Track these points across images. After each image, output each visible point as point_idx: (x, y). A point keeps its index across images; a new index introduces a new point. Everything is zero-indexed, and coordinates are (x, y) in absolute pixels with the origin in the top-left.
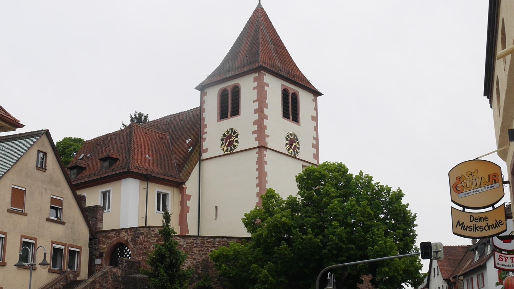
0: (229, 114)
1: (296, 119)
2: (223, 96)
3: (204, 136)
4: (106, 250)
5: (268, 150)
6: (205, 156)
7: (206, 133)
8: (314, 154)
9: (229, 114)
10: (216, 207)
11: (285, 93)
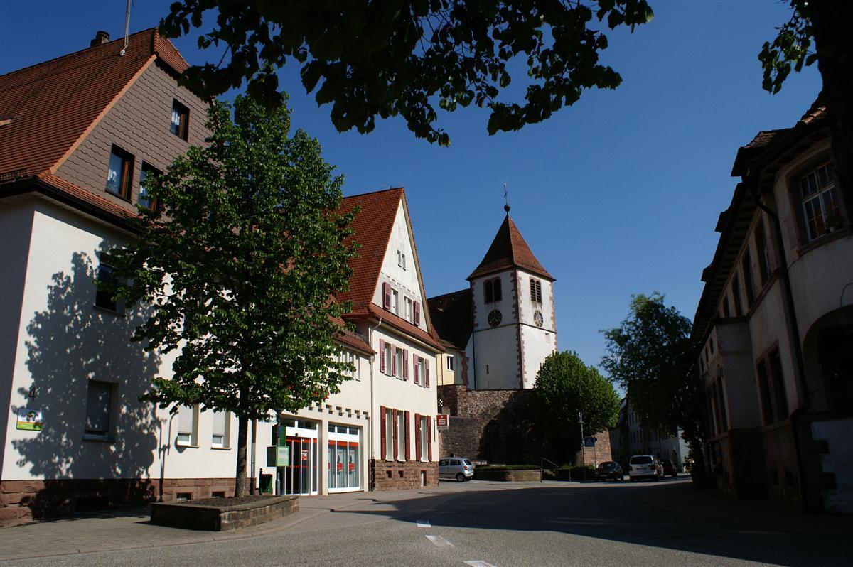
0: (493, 299)
1: (540, 300)
2: (488, 285)
3: (475, 314)
6: (476, 329)
9: (493, 299)
11: (532, 281)
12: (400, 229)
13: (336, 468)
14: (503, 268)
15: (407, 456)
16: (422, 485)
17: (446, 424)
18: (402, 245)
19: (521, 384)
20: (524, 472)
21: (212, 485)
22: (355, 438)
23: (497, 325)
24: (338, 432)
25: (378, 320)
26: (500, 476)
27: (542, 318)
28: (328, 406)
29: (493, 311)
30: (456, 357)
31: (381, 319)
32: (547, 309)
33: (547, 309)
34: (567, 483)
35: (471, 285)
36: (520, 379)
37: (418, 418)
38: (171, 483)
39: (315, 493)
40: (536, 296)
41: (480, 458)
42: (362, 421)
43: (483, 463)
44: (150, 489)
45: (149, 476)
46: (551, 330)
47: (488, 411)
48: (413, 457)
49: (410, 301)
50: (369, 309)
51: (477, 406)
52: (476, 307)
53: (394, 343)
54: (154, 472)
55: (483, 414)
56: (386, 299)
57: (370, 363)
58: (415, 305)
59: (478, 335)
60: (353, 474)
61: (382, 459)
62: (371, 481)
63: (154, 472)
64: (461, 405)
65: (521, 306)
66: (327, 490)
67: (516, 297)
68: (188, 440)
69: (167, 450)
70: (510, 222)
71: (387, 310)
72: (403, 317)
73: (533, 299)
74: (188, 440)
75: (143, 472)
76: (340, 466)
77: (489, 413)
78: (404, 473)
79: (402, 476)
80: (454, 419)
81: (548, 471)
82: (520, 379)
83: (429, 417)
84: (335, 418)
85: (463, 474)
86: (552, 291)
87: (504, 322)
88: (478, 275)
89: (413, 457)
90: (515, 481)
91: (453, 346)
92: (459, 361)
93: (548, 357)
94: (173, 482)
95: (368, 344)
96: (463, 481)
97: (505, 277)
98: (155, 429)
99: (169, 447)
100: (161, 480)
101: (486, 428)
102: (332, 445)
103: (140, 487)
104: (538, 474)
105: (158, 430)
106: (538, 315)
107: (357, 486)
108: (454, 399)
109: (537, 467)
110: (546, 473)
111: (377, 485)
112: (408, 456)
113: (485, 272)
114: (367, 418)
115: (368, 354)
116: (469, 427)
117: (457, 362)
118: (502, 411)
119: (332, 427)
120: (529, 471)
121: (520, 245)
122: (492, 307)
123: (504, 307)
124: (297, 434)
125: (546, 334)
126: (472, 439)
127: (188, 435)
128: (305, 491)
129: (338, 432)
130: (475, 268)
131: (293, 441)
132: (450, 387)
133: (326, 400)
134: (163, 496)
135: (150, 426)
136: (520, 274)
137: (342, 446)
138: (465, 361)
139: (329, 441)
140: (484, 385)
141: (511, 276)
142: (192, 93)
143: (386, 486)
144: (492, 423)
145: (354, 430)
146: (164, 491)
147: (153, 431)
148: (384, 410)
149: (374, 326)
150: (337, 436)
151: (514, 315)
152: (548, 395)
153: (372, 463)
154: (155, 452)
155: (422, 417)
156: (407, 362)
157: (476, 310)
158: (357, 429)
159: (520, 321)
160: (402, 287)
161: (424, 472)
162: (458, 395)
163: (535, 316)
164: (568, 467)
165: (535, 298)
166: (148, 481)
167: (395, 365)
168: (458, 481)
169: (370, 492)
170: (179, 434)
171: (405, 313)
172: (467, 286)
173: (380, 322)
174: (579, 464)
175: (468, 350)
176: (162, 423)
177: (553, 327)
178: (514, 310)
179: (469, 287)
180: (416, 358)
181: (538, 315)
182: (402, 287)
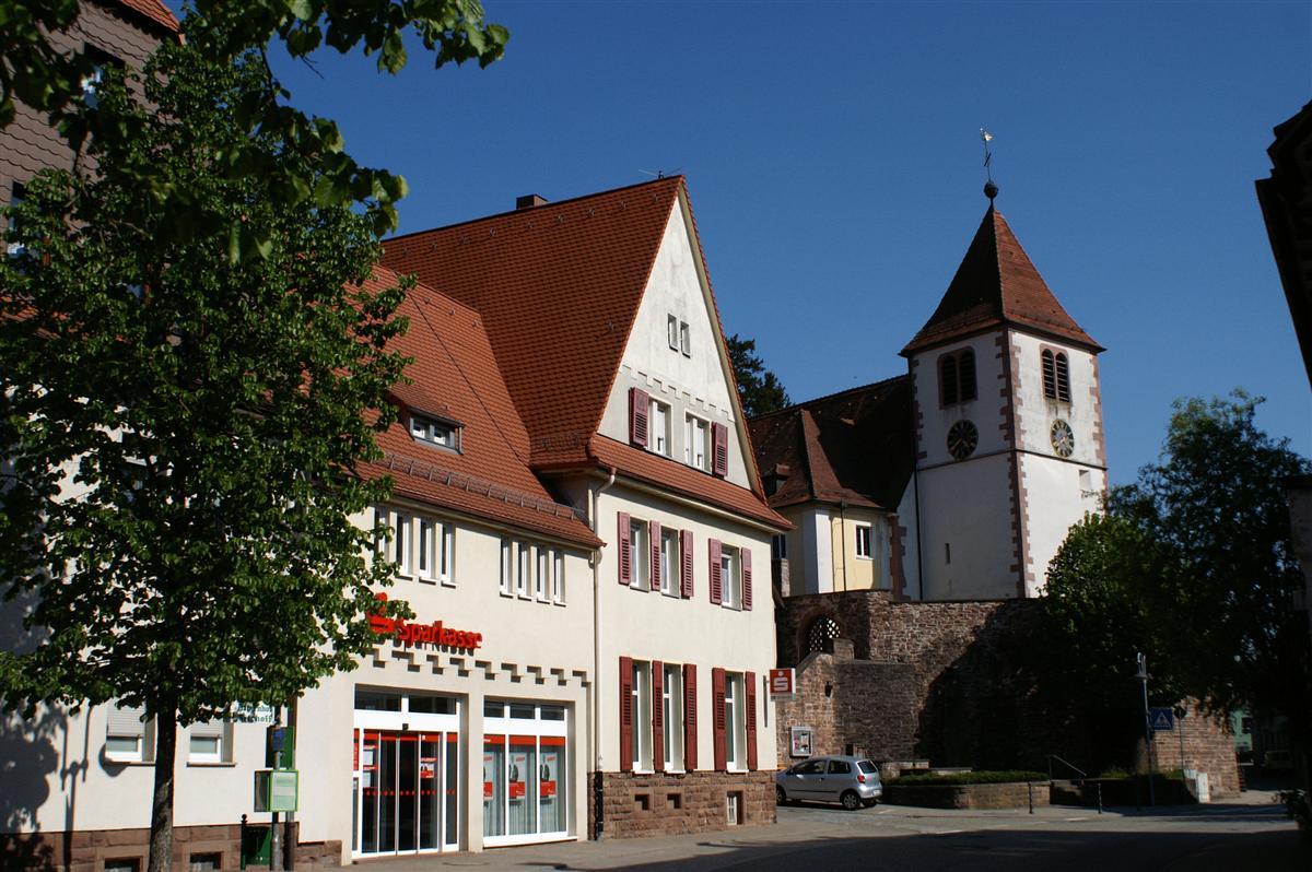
0: (959, 396)
1: (1065, 396)
2: (946, 364)
3: (919, 431)
4: (799, 626)
5: (1026, 454)
6: (922, 463)
7: (922, 427)
8: (1260, 185)
9: (959, 396)
10: (947, 545)
11: (1046, 353)
12: (674, 266)
13: (509, 794)
14: (976, 327)
15: (690, 759)
16: (732, 822)
17: (790, 690)
18: (681, 302)
19: (1021, 585)
20: (1002, 787)
21: (191, 839)
22: (557, 728)
23: (967, 454)
24: (542, 718)
25: (609, 472)
26: (941, 796)
27: (1071, 437)
28: (479, 664)
29: (958, 425)
30: (877, 526)
31: (614, 470)
32: (1083, 415)
33: (1083, 415)
34: (1092, 813)
35: (911, 365)
36: (1017, 574)
37: (722, 680)
38: (91, 840)
39: (455, 848)
40: (1057, 385)
41: (919, 753)
42: (573, 692)
43: (918, 766)
44: (41, 852)
45: (38, 826)
46: (1094, 462)
47: (937, 647)
48: (706, 761)
49: (702, 424)
50: (588, 451)
51: (914, 636)
52: (921, 416)
53: (656, 520)
54: (50, 818)
55: (928, 655)
56: (638, 424)
57: (592, 566)
58: (715, 432)
59: (925, 477)
60: (554, 804)
61: (622, 771)
62: (593, 819)
63: (50, 818)
64: (878, 634)
65: (1021, 411)
66: (479, 839)
67: (1008, 392)
68: (136, 750)
69: (81, 772)
70: (997, 223)
71: (640, 447)
72: (687, 461)
73: (1049, 393)
74: (136, 750)
75: (24, 821)
76: (517, 788)
77: (941, 652)
78: (683, 799)
79: (677, 806)
80: (861, 667)
81: (1066, 785)
82: (1017, 574)
83: (751, 676)
84: (503, 687)
85: (855, 793)
86: (1096, 375)
87: (980, 449)
88: (924, 343)
89: (706, 761)
90: (978, 808)
91: (871, 504)
92: (884, 536)
93: (1075, 526)
94: (96, 837)
95: (586, 523)
96: (857, 808)
97: (983, 347)
98: (53, 732)
99: (85, 765)
100: (68, 835)
101: (934, 686)
102: (494, 745)
103: (17, 850)
104: (1043, 791)
105: (59, 732)
106: (1061, 431)
107: (561, 828)
108: (862, 622)
109: (1039, 775)
110: (1060, 790)
111: (609, 825)
112: (690, 760)
113: (940, 337)
114: (585, 684)
115: (588, 547)
116: (894, 685)
117: (880, 539)
118: (971, 647)
119: (493, 707)
120: (1016, 785)
121: (1020, 273)
122: (956, 414)
123: (982, 413)
124: (405, 726)
125: (1082, 472)
126: (901, 710)
127: (135, 739)
128: (428, 841)
129: (542, 718)
130: (920, 327)
131: (398, 741)
132: (854, 597)
133: (476, 650)
134: (72, 867)
135: (41, 725)
136: (1018, 339)
137: (523, 745)
138: (897, 535)
139: (486, 736)
140: (938, 588)
141: (997, 344)
142: (139, 32)
143: (634, 827)
144: (947, 676)
145: (553, 710)
146: (74, 857)
147: (48, 735)
148: (630, 669)
149: (600, 485)
150: (507, 726)
151: (1005, 432)
152: (1071, 613)
153: (597, 780)
154: (53, 779)
155: (732, 676)
156: (690, 558)
157: (921, 422)
158: (563, 708)
159: (1018, 446)
160: (680, 395)
161: (739, 794)
162: (869, 614)
163: (1054, 433)
164: (1115, 775)
165: (1053, 393)
166: (37, 837)
167: (654, 563)
168: (844, 808)
169: (593, 842)
170: (109, 738)
171: (690, 449)
172: (901, 368)
173: (613, 477)
174: (1143, 769)
175: (905, 512)
176: (70, 720)
177: (1098, 457)
178: (1003, 420)
179: (906, 372)
180: (717, 548)
181: (1061, 431)
182: (680, 395)
